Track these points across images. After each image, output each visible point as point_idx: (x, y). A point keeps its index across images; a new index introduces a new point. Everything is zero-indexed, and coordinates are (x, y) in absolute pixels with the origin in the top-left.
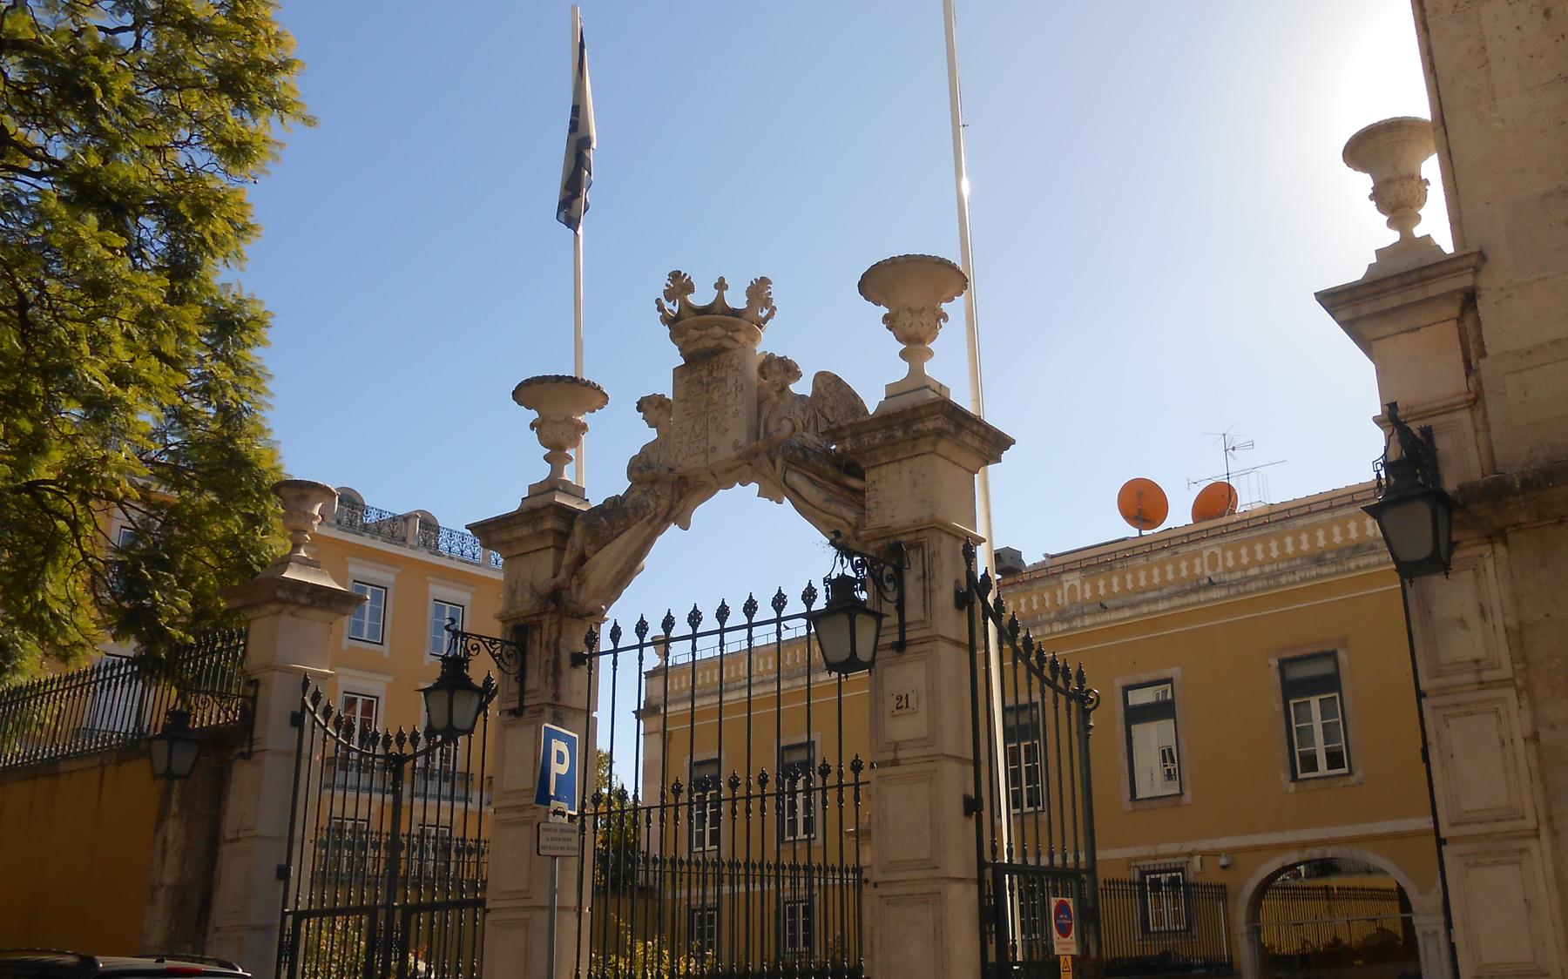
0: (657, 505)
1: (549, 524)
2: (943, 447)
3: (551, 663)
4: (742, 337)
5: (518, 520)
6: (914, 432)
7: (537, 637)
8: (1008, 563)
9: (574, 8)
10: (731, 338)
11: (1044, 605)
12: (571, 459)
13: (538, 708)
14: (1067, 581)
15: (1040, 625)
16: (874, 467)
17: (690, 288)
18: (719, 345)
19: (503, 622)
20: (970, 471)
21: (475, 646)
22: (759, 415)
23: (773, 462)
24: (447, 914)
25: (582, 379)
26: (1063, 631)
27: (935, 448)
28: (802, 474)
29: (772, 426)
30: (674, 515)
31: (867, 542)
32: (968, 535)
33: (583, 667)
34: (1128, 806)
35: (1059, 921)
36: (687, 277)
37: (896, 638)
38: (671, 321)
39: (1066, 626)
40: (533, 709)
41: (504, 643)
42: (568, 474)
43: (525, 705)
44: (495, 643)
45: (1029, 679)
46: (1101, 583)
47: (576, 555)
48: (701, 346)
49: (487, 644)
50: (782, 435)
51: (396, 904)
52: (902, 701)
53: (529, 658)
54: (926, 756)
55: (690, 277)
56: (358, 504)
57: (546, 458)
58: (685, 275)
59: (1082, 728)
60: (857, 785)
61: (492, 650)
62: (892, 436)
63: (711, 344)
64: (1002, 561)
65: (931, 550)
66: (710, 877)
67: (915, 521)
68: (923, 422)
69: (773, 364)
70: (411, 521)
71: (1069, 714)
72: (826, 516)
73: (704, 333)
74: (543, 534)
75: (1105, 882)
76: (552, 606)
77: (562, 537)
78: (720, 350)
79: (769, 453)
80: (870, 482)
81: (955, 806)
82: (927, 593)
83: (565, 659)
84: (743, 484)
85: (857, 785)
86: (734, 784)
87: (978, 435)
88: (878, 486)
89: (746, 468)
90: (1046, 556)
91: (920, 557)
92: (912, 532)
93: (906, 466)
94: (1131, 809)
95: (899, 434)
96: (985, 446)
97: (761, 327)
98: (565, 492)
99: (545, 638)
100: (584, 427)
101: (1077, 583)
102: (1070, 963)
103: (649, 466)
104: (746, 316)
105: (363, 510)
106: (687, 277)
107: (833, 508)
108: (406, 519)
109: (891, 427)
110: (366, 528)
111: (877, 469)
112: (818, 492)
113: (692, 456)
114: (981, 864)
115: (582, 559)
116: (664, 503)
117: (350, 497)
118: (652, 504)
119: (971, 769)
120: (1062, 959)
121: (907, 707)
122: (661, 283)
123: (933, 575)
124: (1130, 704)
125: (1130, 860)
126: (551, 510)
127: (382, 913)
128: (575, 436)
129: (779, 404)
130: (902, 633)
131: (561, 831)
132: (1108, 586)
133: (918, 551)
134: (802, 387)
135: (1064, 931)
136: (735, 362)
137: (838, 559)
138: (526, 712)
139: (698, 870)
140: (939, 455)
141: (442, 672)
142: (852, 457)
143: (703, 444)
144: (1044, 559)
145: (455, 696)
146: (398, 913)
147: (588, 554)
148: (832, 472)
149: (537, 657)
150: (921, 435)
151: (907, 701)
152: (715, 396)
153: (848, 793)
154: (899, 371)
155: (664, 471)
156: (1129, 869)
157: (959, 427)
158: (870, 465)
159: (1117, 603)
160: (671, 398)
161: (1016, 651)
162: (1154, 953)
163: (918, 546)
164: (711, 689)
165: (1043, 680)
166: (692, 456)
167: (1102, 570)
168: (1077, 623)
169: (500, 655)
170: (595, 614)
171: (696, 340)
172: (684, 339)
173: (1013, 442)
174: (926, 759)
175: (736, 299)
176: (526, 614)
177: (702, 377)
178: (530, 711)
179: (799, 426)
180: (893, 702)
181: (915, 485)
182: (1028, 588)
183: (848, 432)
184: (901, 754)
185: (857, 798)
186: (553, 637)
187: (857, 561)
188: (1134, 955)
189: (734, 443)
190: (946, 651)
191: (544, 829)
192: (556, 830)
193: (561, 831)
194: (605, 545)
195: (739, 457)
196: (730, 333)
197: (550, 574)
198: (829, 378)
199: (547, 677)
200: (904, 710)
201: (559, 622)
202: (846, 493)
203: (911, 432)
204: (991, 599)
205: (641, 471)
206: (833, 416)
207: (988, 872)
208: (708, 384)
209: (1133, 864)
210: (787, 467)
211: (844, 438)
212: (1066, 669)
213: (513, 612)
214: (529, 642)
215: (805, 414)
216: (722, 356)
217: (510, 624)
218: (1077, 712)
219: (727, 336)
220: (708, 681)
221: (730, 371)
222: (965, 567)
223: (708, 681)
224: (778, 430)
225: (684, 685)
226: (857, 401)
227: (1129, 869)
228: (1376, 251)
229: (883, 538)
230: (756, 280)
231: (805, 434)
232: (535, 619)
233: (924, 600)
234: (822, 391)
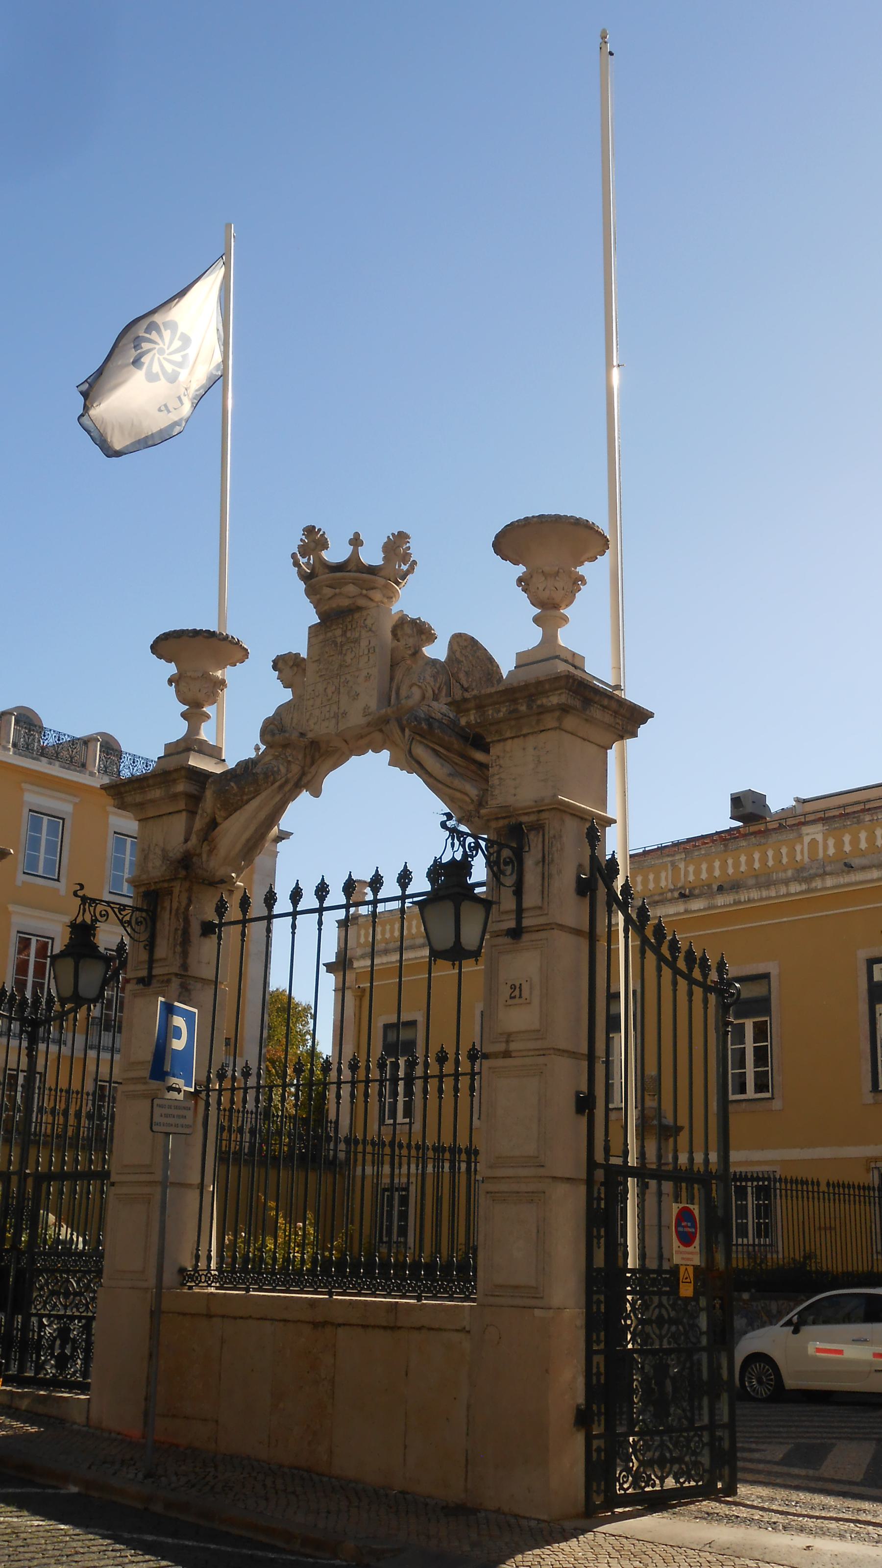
0: (288, 771)
1: (181, 787)
2: (570, 722)
3: (180, 932)
4: (377, 596)
5: (151, 782)
6: (539, 706)
7: (167, 904)
8: (749, 808)
9: (228, 226)
10: (366, 596)
11: (780, 861)
12: (208, 717)
13: (166, 978)
14: (808, 834)
15: (775, 884)
16: (499, 741)
17: (323, 544)
18: (354, 604)
19: (135, 886)
20: (602, 747)
21: (103, 913)
22: (392, 679)
23: (403, 730)
24: (89, 1184)
25: (221, 634)
26: (801, 892)
27: (560, 724)
28: (427, 746)
29: (403, 692)
30: (306, 781)
31: (488, 820)
32: (594, 816)
33: (212, 936)
34: (869, 1098)
35: (680, 1229)
36: (321, 533)
37: (512, 924)
38: (305, 577)
39: (804, 887)
40: (161, 978)
41: (135, 909)
42: (206, 733)
43: (154, 973)
44: (124, 910)
45: (659, 970)
46: (847, 838)
47: (207, 820)
48: (334, 606)
49: (116, 910)
50: (411, 703)
51: (27, 1171)
52: (516, 991)
53: (159, 925)
54: (538, 1050)
55: (324, 532)
56: (36, 726)
57: (184, 715)
58: (319, 530)
59: (720, 1024)
60: (473, 1075)
61: (120, 917)
62: (516, 711)
63: (345, 602)
64: (742, 806)
65: (552, 832)
66: (369, 1157)
67: (536, 802)
68: (548, 697)
69: (406, 626)
70: (90, 745)
71: (706, 1008)
72: (451, 791)
73: (337, 591)
74: (175, 797)
75: (828, 1184)
76: (183, 873)
77: (194, 800)
78: (353, 610)
79: (399, 721)
80: (494, 758)
81: (566, 1103)
82: (545, 878)
83: (195, 928)
84: (376, 751)
85: (473, 1075)
86: (442, 1058)
87: (609, 709)
88: (502, 762)
89: (378, 736)
90: (797, 800)
91: (541, 839)
92: (533, 812)
93: (531, 741)
94: (872, 1101)
95: (523, 708)
96: (618, 721)
97: (398, 584)
98: (200, 752)
99: (175, 905)
100: (222, 684)
101: (819, 838)
102: (692, 1276)
103: (282, 730)
104: (382, 573)
105: (41, 732)
106: (321, 533)
107: (457, 783)
108: (86, 742)
109: (514, 701)
110: (43, 752)
111: (502, 744)
112: (443, 765)
113: (324, 720)
114: (591, 1164)
115: (213, 824)
116: (295, 769)
117: (28, 717)
118: (283, 770)
119: (585, 1064)
120: (682, 1269)
121: (520, 997)
122: (295, 540)
123: (553, 860)
124: (875, 980)
125: (869, 1160)
126: (183, 773)
127: (14, 1179)
128: (213, 692)
129: (412, 667)
130: (519, 919)
131: (176, 1107)
132: (855, 842)
133: (539, 832)
134: (437, 651)
135: (686, 1240)
136: (369, 622)
137: (450, 841)
138: (154, 981)
139: (374, 1150)
140: (566, 731)
141: (71, 938)
142: (477, 730)
143: (334, 708)
144: (794, 803)
145: (80, 965)
146: (30, 1181)
147: (219, 820)
148: (457, 744)
149: (167, 925)
150: (544, 710)
151: (521, 991)
152: (348, 658)
153: (464, 1082)
154: (533, 637)
155: (295, 736)
156: (868, 1170)
157: (587, 702)
158: (495, 739)
159: (864, 861)
160: (306, 657)
161: (645, 941)
162: (855, 1268)
163: (538, 827)
164: (392, 945)
165: (676, 972)
166: (324, 720)
167: (849, 823)
168: (818, 883)
169: (129, 923)
170: (225, 882)
171: (330, 599)
172: (318, 596)
173: (651, 715)
174: (537, 1053)
175: (371, 556)
176: (157, 880)
177: (335, 637)
178: (158, 981)
179: (429, 694)
180: (506, 991)
181: (539, 762)
182: (763, 841)
183: (472, 704)
184: (513, 1046)
185: (472, 1089)
186: (184, 904)
187: (470, 844)
188: (860, 1269)
189: (365, 708)
190: (564, 942)
191: (159, 1106)
192: (170, 1107)
193: (176, 1107)
194: (235, 810)
195: (369, 724)
196: (364, 592)
197: (182, 839)
198: (465, 640)
199: (175, 946)
200: (517, 1001)
201: (190, 890)
202: (473, 767)
203: (535, 707)
204: (620, 882)
205: (273, 735)
206: (468, 682)
207: (600, 1175)
208: (342, 646)
209: (873, 1165)
210: (413, 738)
211: (468, 710)
212: (704, 960)
213: (144, 877)
214: (159, 909)
215: (435, 681)
216: (357, 616)
217: (142, 889)
218: (717, 1006)
219: (361, 594)
220: (387, 936)
221: (363, 632)
222: (588, 852)
223: (387, 936)
224: (408, 697)
225: (362, 940)
226: (492, 665)
227: (868, 1170)
228: (389, 765)
229: (504, 818)
230: (393, 534)
231: (435, 704)
232: (166, 885)
233: (543, 885)
234: (458, 654)
